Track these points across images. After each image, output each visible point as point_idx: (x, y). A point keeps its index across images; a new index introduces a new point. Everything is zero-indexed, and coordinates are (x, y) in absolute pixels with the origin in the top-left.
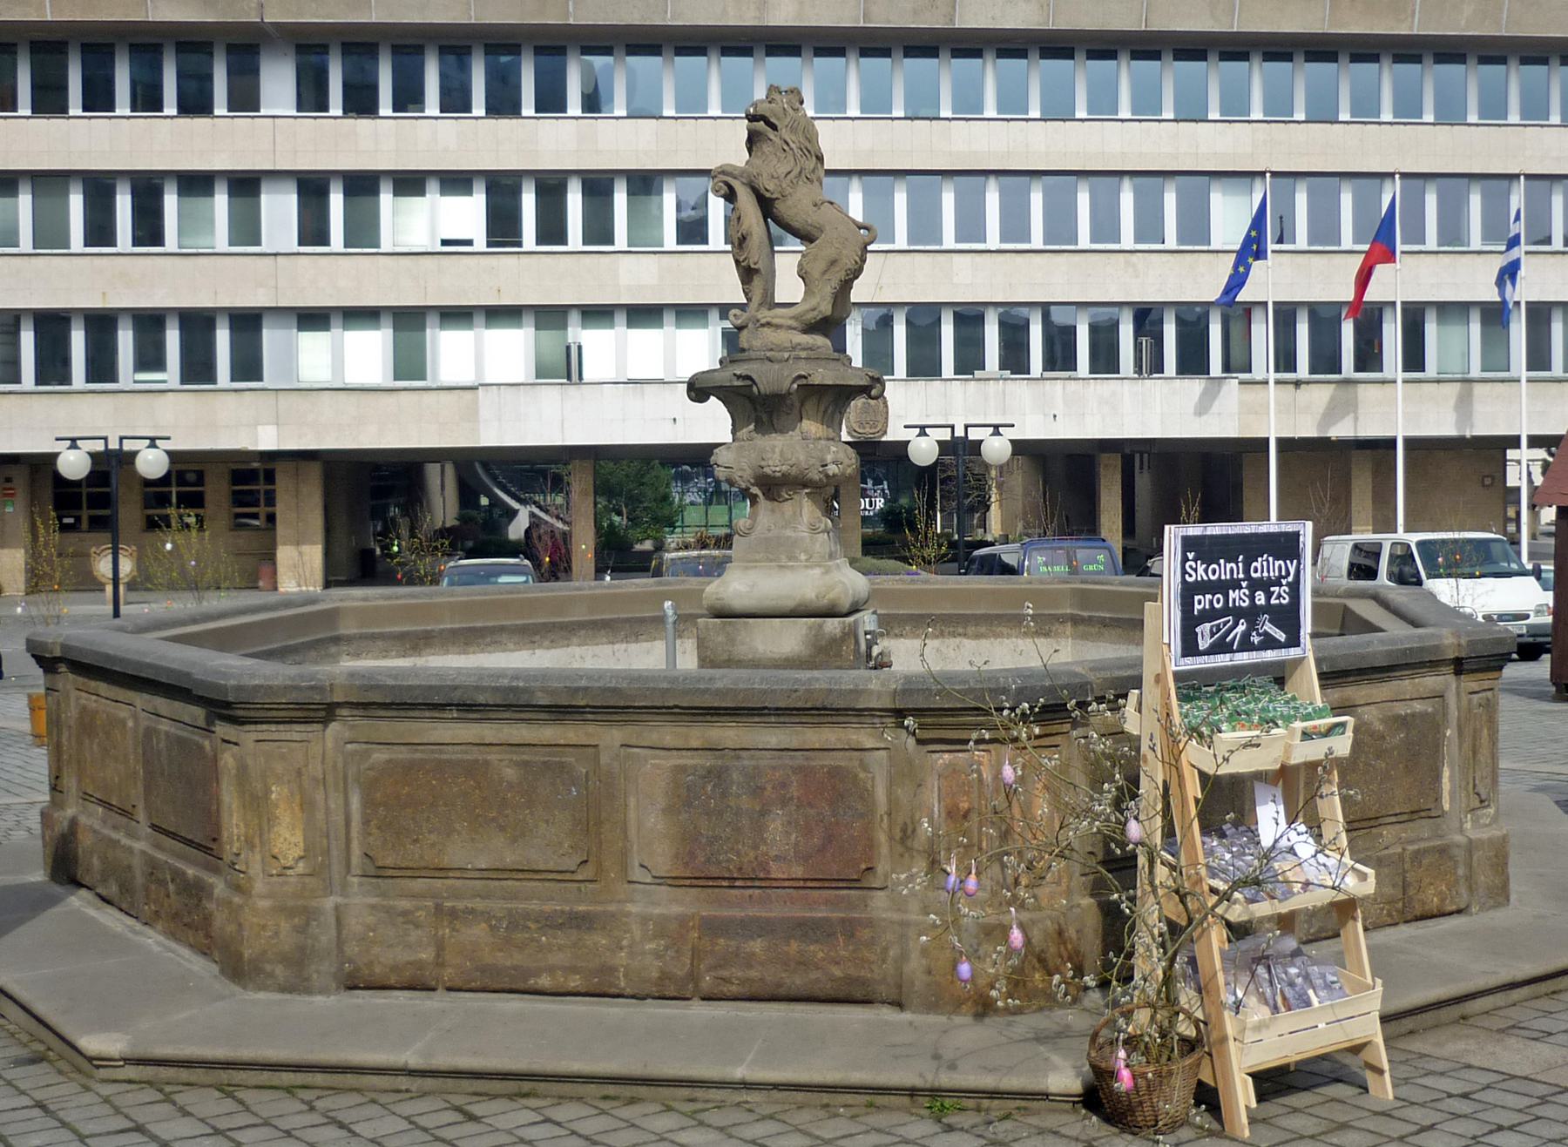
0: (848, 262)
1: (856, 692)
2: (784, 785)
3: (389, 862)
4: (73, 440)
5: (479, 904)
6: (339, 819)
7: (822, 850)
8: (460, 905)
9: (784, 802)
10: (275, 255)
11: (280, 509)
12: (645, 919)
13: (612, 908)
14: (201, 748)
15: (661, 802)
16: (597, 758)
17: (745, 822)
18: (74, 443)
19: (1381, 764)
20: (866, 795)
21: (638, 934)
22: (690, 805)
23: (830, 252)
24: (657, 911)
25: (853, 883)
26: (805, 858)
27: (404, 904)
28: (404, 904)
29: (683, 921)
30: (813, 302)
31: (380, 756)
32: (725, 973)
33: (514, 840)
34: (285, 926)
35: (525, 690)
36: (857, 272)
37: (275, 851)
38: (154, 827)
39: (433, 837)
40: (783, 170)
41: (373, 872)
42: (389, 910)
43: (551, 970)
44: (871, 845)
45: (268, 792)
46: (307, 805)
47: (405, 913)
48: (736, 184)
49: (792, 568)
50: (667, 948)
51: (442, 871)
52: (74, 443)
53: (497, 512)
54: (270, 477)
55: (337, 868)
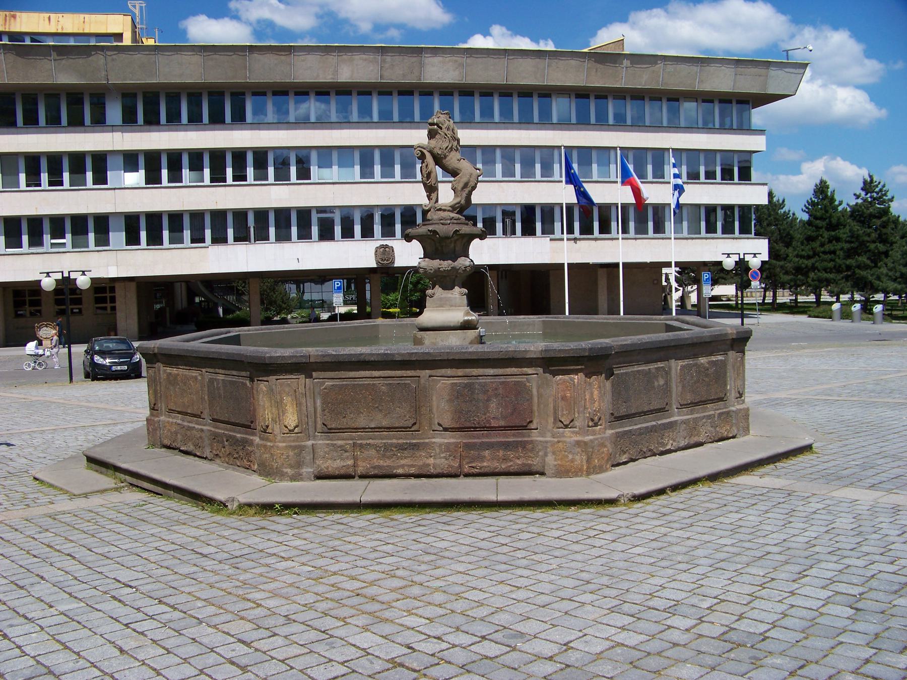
0: (472, 184)
1: (526, 351)
2: (496, 389)
3: (333, 426)
4: (48, 273)
5: (371, 441)
6: (311, 409)
7: (512, 414)
8: (364, 442)
9: (496, 396)
10: (115, 189)
11: (118, 304)
12: (440, 445)
13: (427, 441)
14: (245, 384)
15: (447, 397)
16: (419, 381)
17: (481, 404)
18: (48, 274)
19: (707, 379)
20: (529, 391)
21: (438, 451)
22: (458, 398)
23: (465, 180)
24: (446, 441)
25: (525, 428)
26: (504, 418)
27: (340, 442)
28: (340, 442)
29: (456, 445)
30: (458, 200)
31: (329, 383)
32: (473, 465)
33: (385, 415)
34: (291, 453)
35: (390, 354)
36: (474, 188)
37: (286, 423)
38: (214, 420)
39: (352, 415)
40: (445, 146)
41: (327, 430)
42: (333, 445)
43: (403, 466)
44: (532, 412)
45: (282, 400)
46: (299, 405)
47: (341, 446)
48: (425, 151)
49: (447, 309)
50: (450, 456)
51: (356, 429)
52: (48, 274)
53: (211, 305)
54: (113, 289)
55: (311, 430)
